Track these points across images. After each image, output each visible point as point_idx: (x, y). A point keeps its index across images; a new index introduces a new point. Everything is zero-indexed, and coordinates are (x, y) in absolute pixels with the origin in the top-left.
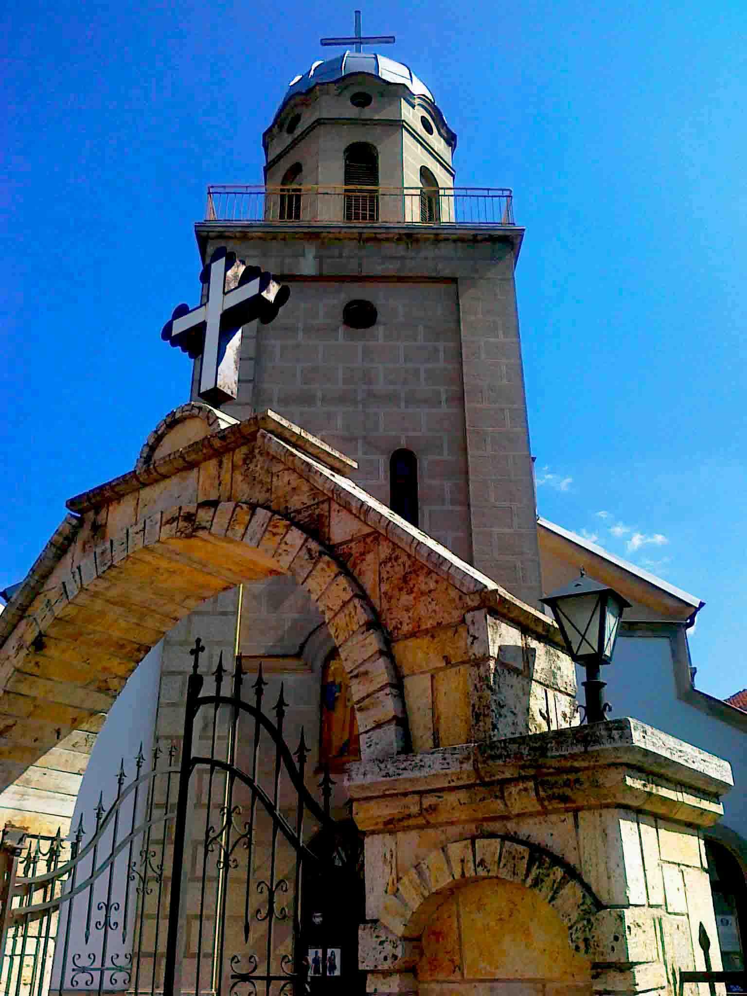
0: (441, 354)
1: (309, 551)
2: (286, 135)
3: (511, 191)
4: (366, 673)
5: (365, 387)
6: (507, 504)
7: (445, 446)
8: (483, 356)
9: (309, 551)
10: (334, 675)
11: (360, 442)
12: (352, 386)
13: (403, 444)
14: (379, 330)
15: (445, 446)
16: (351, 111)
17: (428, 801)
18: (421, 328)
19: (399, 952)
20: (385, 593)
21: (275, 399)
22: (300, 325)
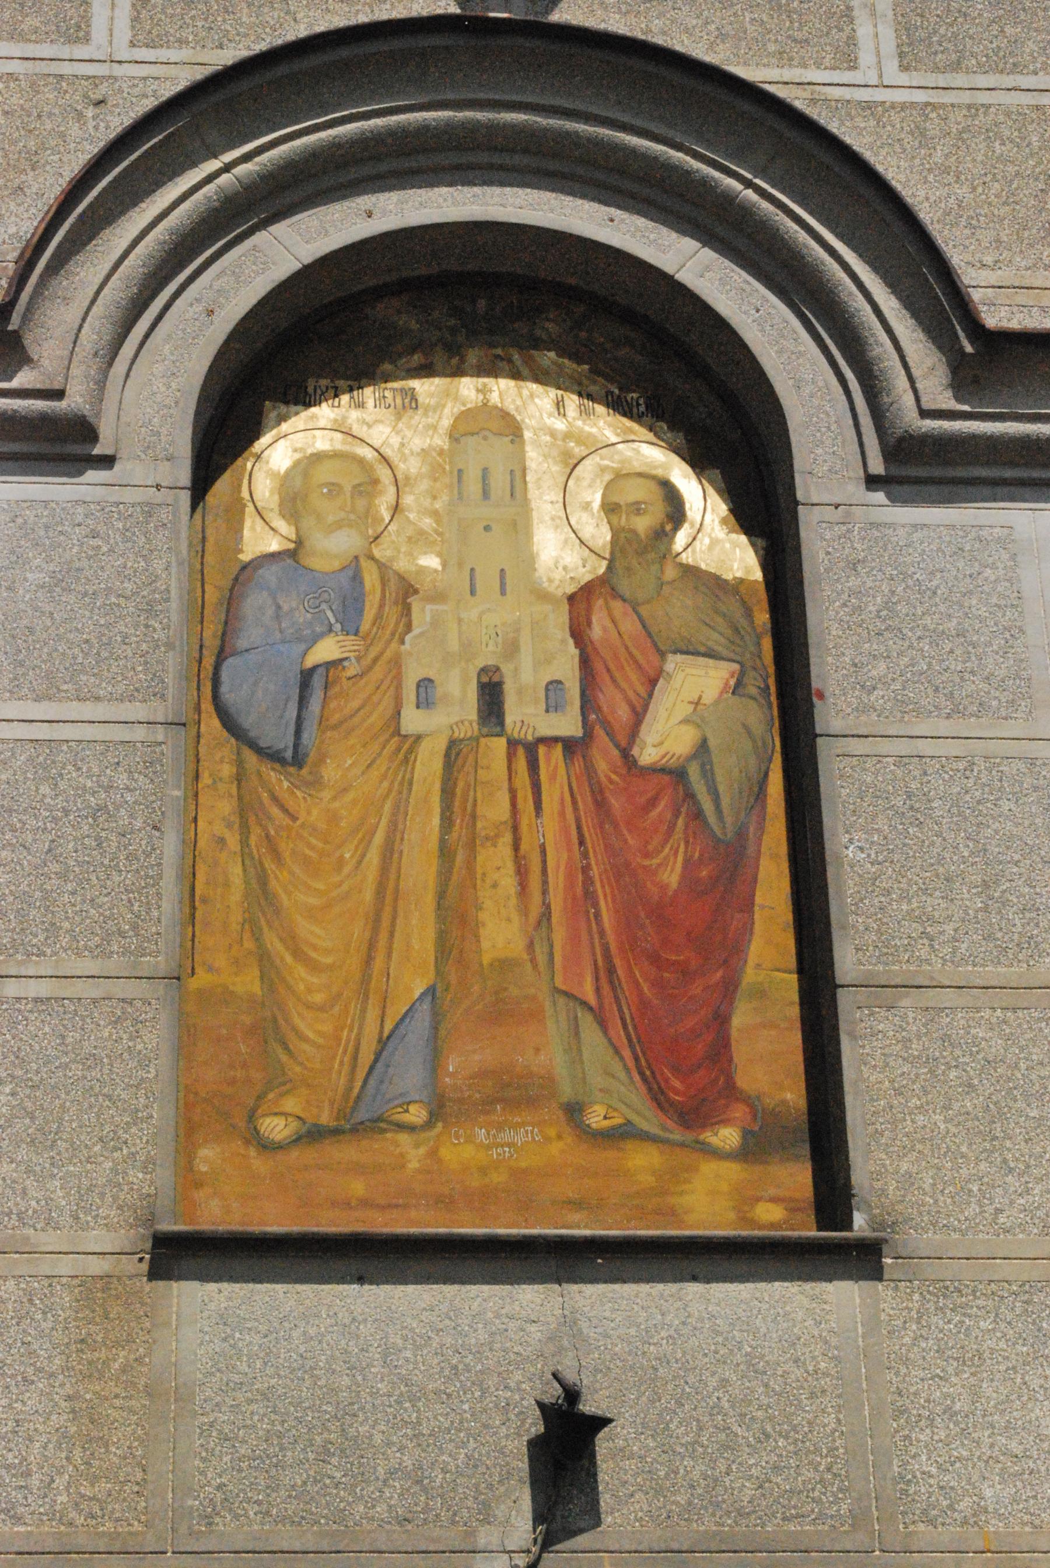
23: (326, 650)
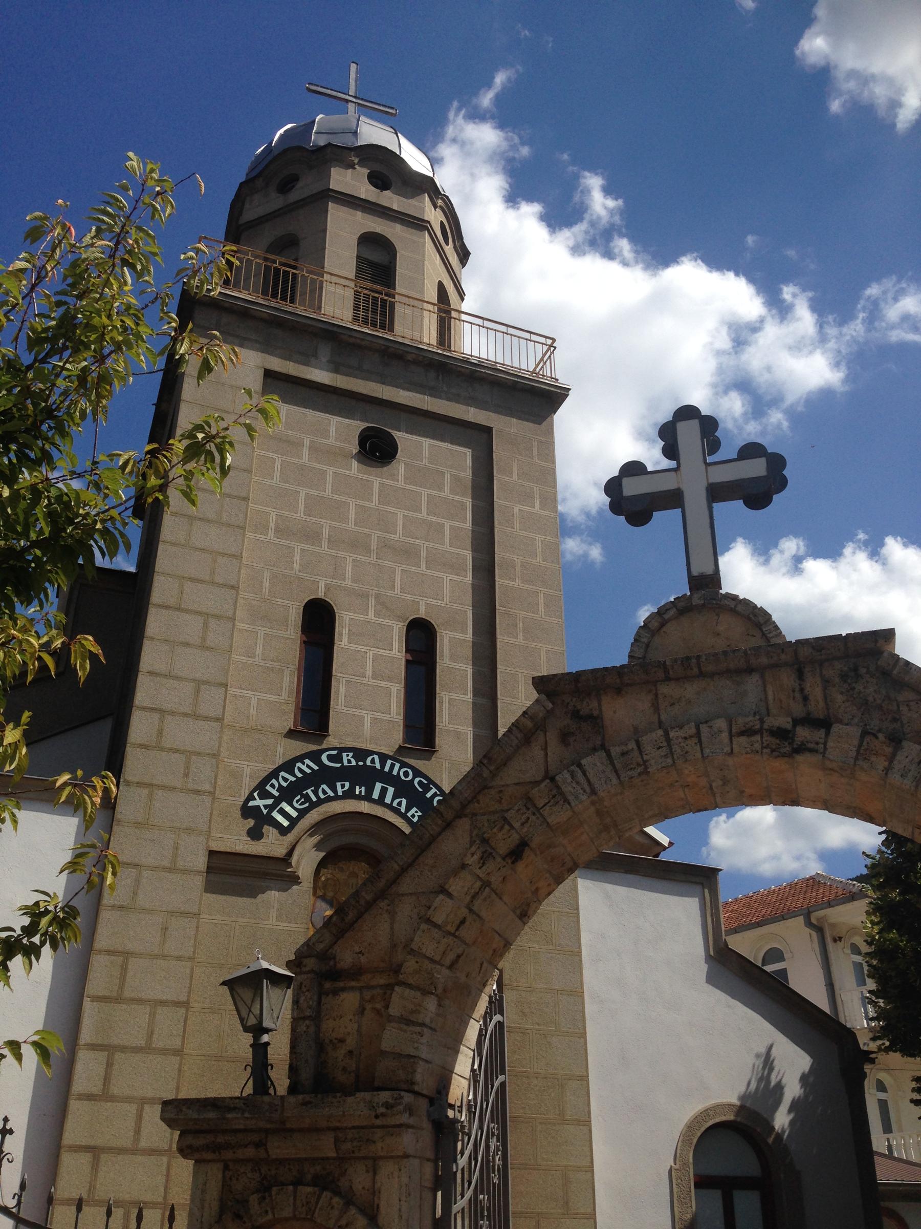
3: (554, 340)
12: (366, 531)
13: (422, 613)
16: (366, 191)
21: (272, 525)
22: (307, 442)
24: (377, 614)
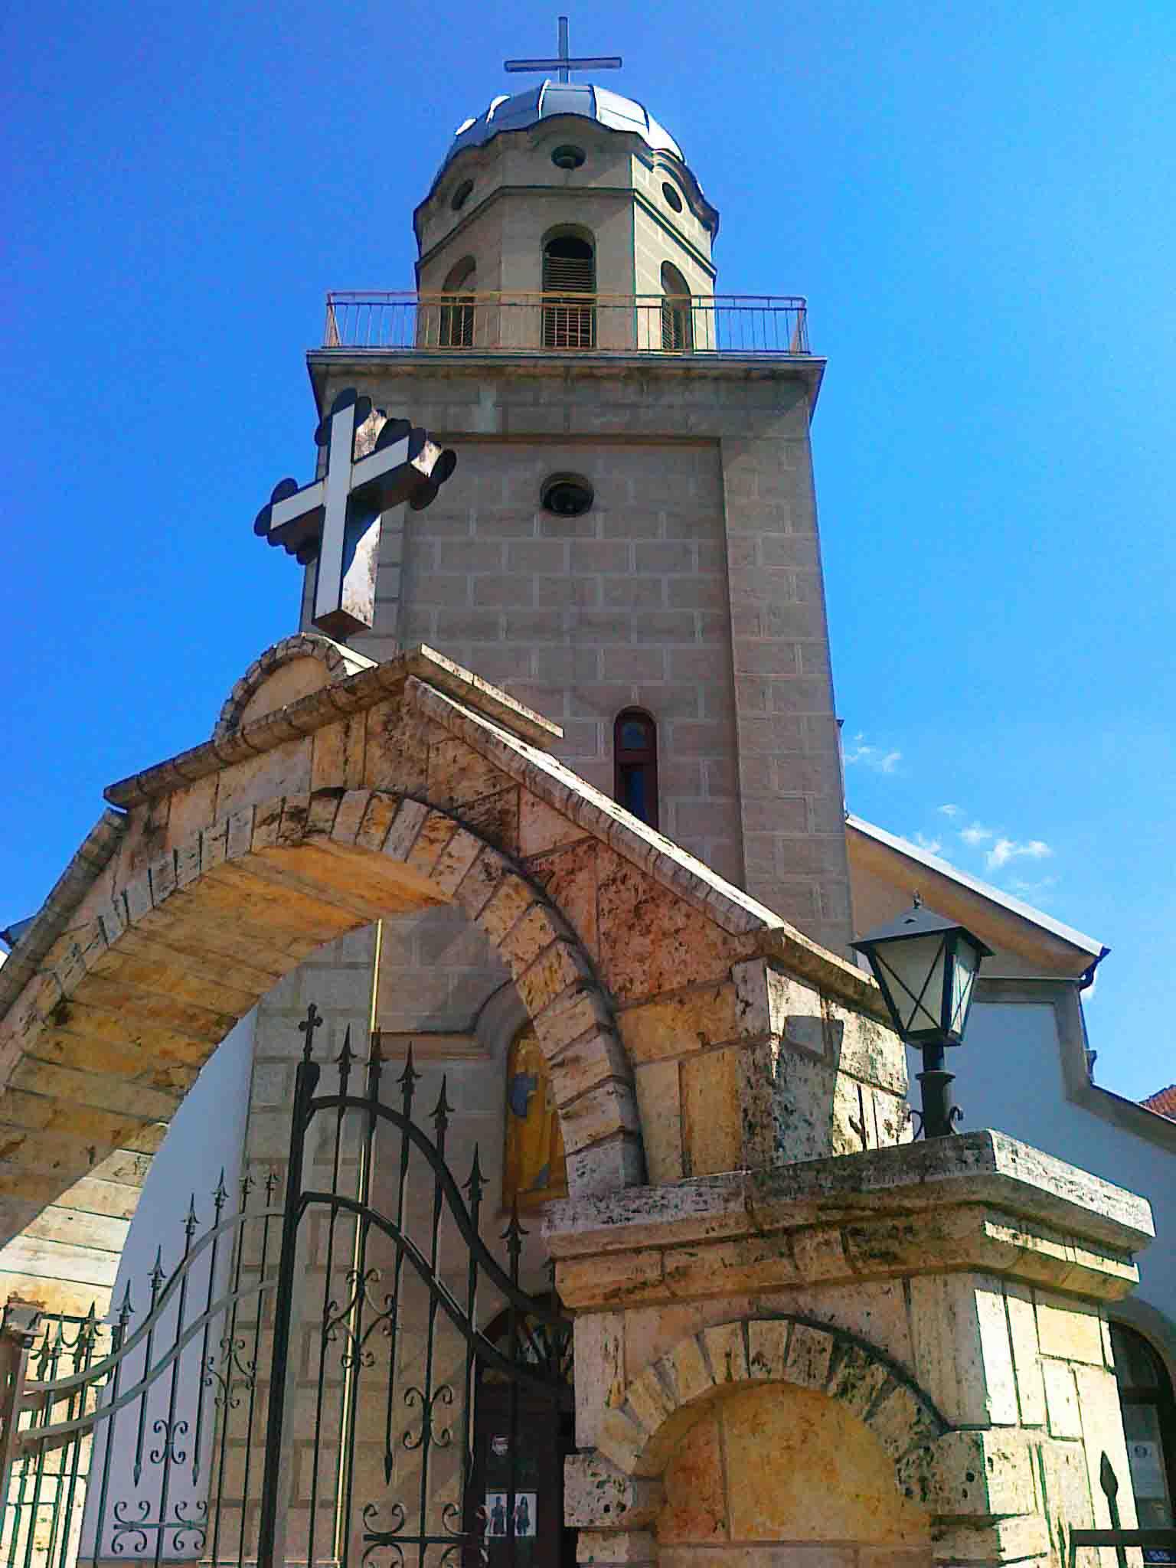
0: (695, 557)
1: (487, 867)
2: (450, 212)
4: (576, 1060)
5: (574, 609)
6: (798, 793)
7: (701, 702)
8: (760, 561)
9: (487, 867)
10: (526, 1062)
11: (567, 695)
13: (635, 699)
14: (596, 520)
15: (701, 702)
16: (553, 175)
17: (673, 1261)
18: (662, 515)
19: (628, 1499)
20: (606, 934)
22: (473, 512)
23: (531, 1093)
24: (575, 714)
